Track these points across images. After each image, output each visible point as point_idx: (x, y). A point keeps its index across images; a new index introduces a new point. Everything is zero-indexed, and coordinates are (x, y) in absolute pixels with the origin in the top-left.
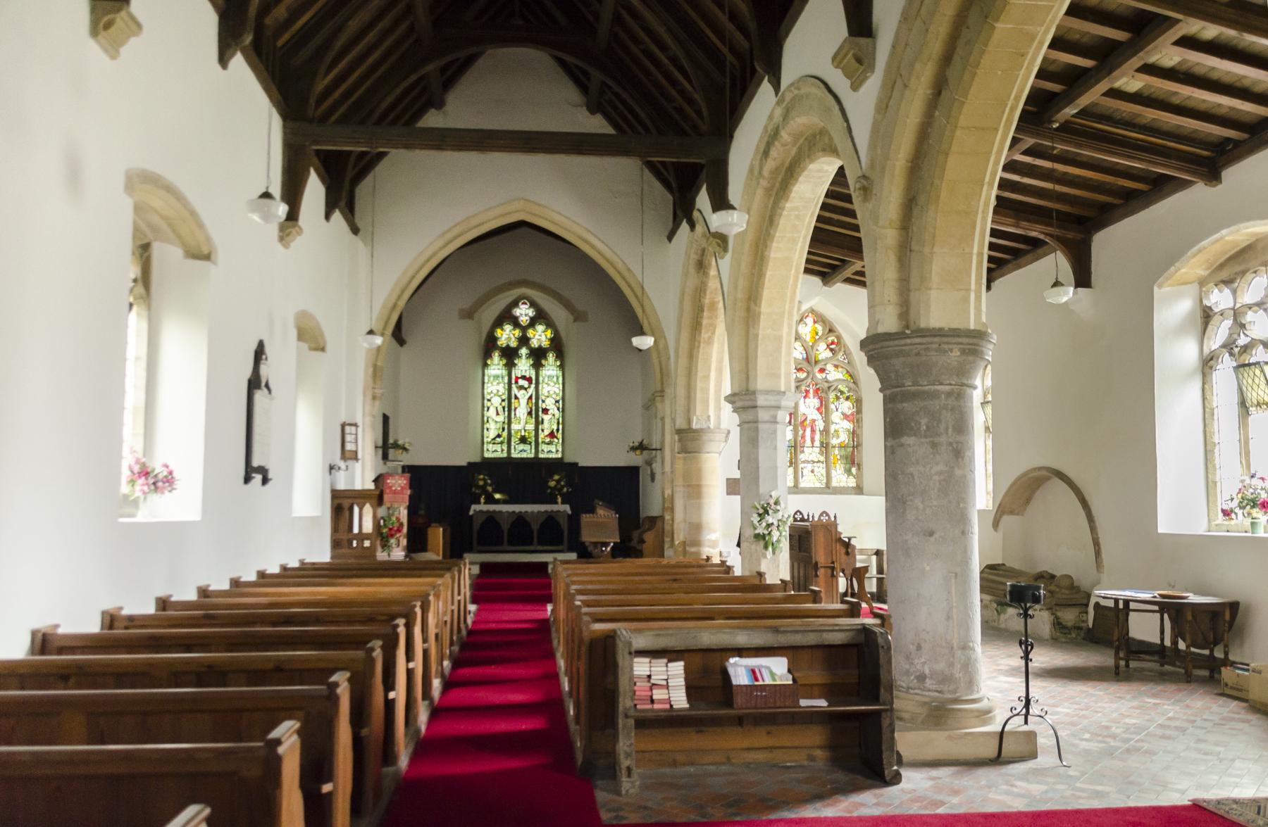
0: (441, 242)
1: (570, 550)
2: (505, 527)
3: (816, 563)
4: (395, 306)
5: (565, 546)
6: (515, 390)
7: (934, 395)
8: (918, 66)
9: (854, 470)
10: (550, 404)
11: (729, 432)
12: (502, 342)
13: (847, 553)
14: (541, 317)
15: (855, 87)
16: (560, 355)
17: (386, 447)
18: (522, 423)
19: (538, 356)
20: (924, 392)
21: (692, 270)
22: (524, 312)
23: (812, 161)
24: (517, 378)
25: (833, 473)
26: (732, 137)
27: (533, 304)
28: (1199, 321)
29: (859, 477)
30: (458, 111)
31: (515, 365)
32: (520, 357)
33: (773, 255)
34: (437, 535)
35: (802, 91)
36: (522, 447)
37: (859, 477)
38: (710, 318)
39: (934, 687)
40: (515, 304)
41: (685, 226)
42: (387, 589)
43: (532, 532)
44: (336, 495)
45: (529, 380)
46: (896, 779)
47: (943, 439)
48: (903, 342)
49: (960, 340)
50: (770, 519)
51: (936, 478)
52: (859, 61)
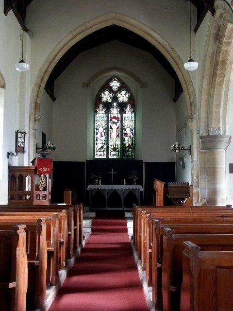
0: (70, 36)
2: (107, 197)
4: (47, 70)
6: (110, 124)
10: (128, 131)
12: (104, 100)
14: (123, 87)
17: (42, 148)
19: (122, 107)
21: (212, 41)
22: (115, 85)
24: (111, 118)
27: (119, 80)
31: (110, 111)
32: (114, 107)
38: (222, 69)
40: (111, 80)
41: (209, 13)
42: (16, 218)
43: (106, 199)
44: (12, 170)
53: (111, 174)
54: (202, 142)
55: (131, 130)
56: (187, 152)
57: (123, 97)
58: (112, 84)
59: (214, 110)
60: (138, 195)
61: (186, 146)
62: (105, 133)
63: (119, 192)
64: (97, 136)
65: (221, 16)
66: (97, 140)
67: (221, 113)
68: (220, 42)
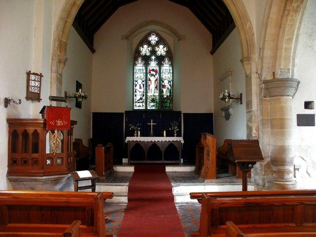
10: (166, 83)
19: (160, 60)
22: (153, 39)
24: (150, 70)
27: (157, 35)
36: (152, 104)
40: (149, 35)
54: (266, 89)
55: (169, 82)
57: (161, 50)
58: (150, 39)
59: (284, 46)
62: (143, 85)
66: (136, 91)
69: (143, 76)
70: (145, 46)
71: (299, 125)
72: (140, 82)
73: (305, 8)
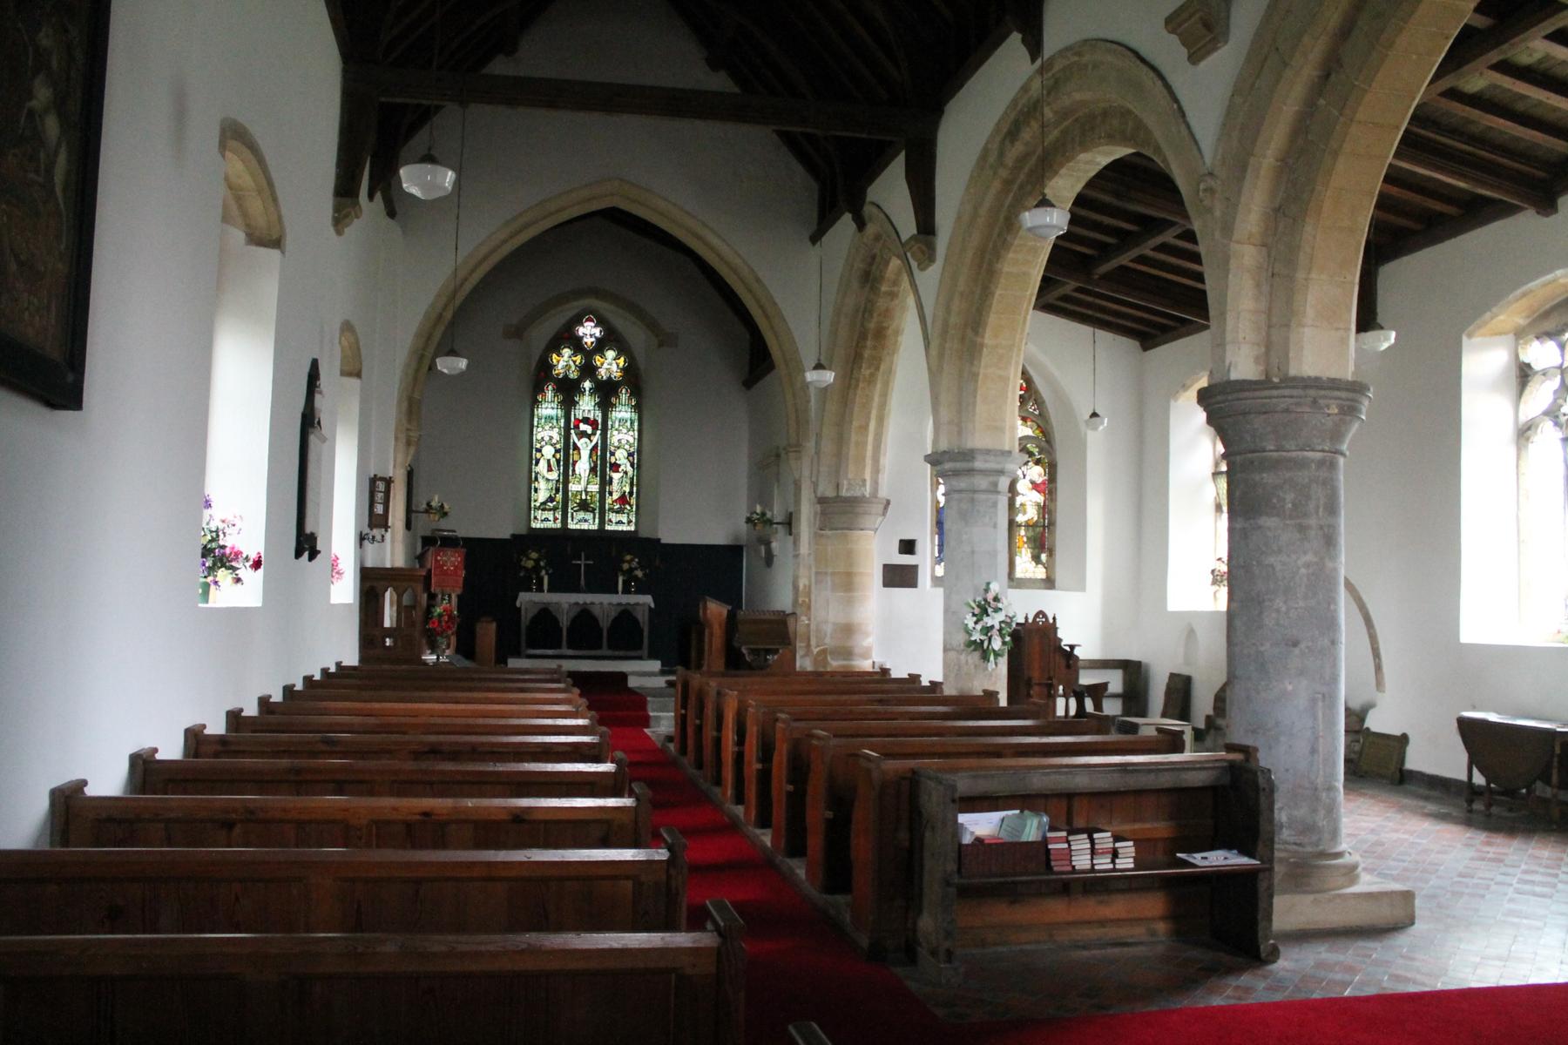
1: (652, 656)
2: (565, 622)
3: (1030, 679)
4: (440, 316)
5: (645, 652)
6: (574, 437)
7: (1302, 464)
8: (1306, 39)
9: (1044, 557)
10: (621, 457)
11: (888, 502)
13: (1068, 666)
15: (1194, 58)
16: (637, 392)
18: (583, 482)
19: (606, 393)
20: (1290, 460)
21: (855, 285)
22: (589, 332)
23: (1085, 149)
24: (578, 421)
25: (1018, 560)
26: (942, 112)
27: (600, 322)
28: (1514, 381)
29: (1049, 568)
30: (536, 56)
32: (582, 393)
33: (1006, 269)
34: (487, 632)
35: (1086, 58)
36: (581, 515)
37: (1049, 568)
39: (1292, 839)
40: (578, 321)
43: (561, 630)
45: (593, 424)
46: (1274, 954)
47: (1313, 522)
48: (1266, 393)
49: (1337, 393)
50: (988, 621)
51: (1303, 571)
52: (1208, 26)
53: (587, 558)
54: (823, 513)
55: (630, 455)
56: (781, 529)
57: (610, 364)
58: (581, 331)
59: (854, 438)
60: (643, 618)
61: (777, 513)
62: (558, 461)
63: (596, 611)
64: (537, 469)
65: (877, 238)
67: (870, 448)
68: (874, 289)
69: (556, 437)
70: (567, 352)
71: (886, 584)
72: (548, 451)
73: (890, 372)
